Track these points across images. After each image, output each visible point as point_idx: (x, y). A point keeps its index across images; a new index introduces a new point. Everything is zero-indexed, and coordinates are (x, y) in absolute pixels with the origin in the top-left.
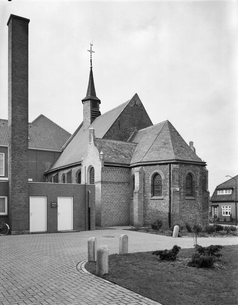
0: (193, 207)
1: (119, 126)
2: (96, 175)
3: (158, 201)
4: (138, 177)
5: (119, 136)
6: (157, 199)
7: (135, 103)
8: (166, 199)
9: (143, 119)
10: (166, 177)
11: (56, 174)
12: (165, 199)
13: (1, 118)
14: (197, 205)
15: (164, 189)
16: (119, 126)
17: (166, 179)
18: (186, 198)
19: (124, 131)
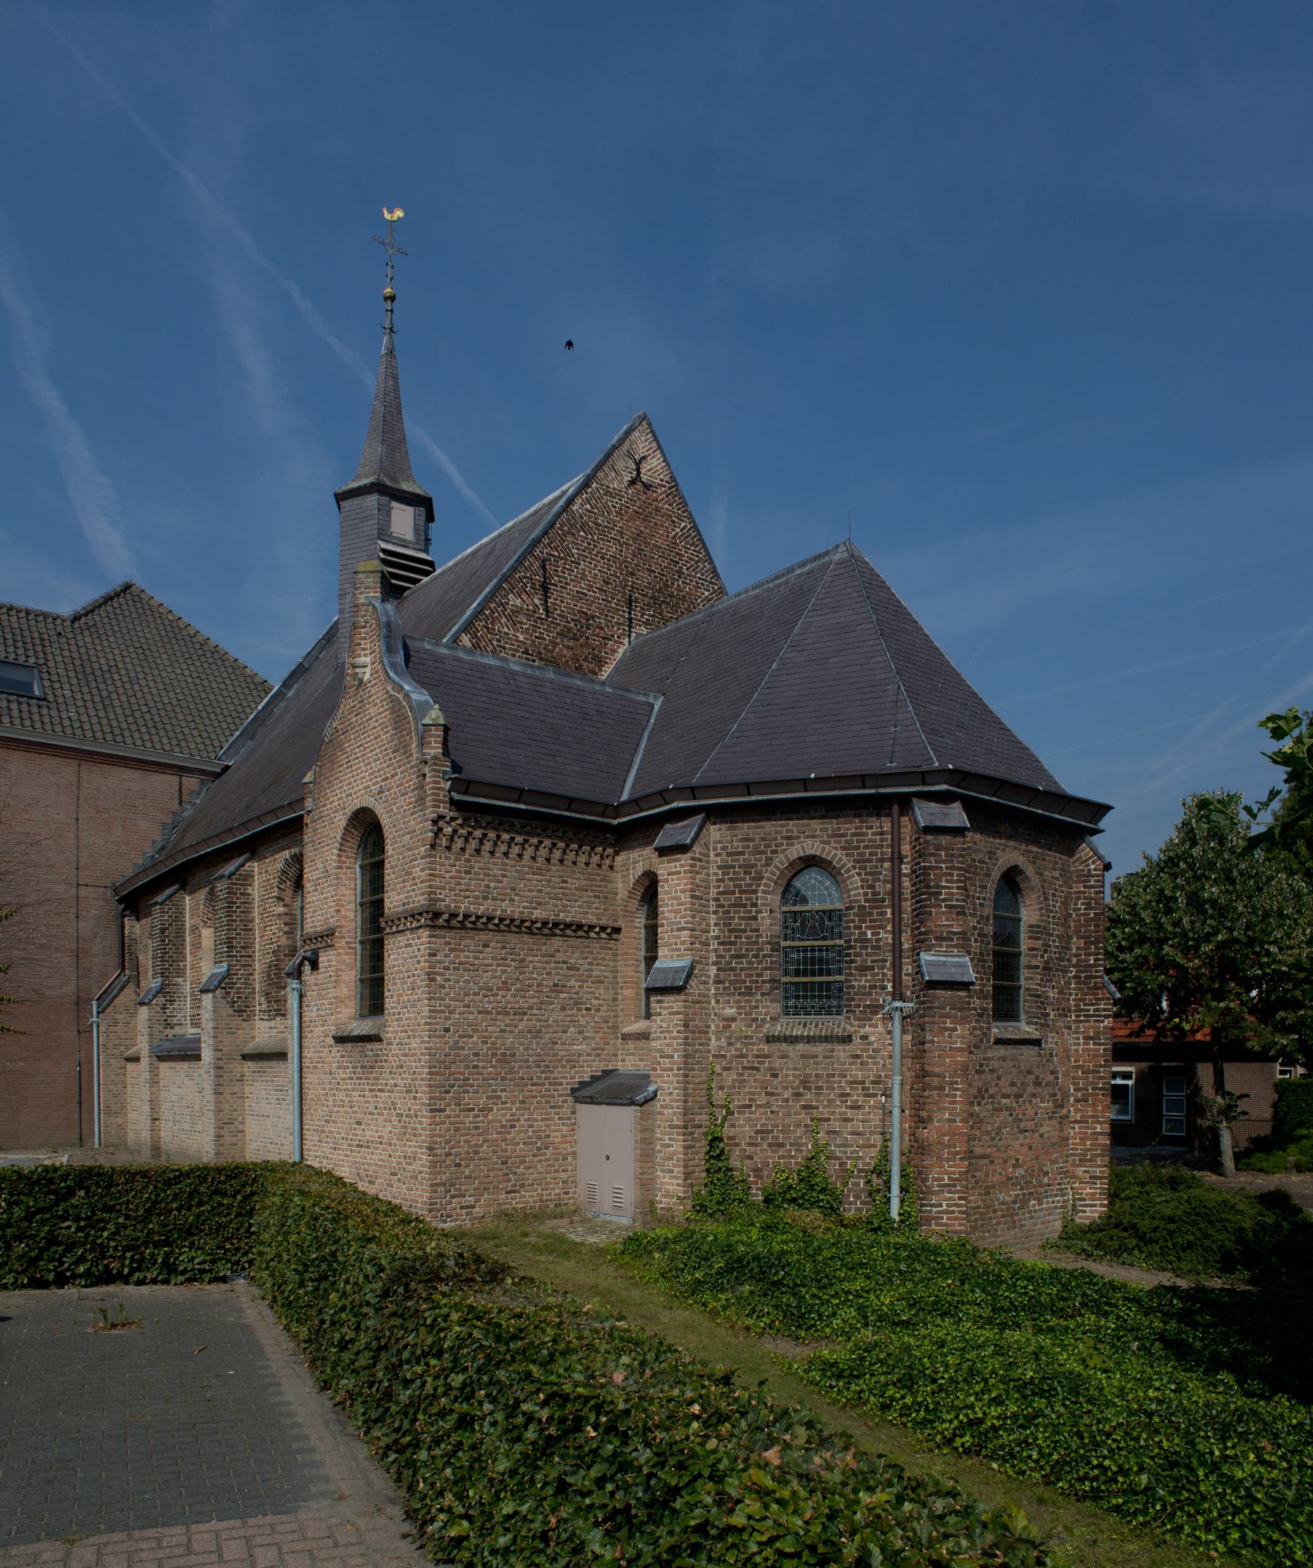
0: (1031, 1089)
1: (546, 598)
2: (1211, 1080)
3: (820, 1048)
4: (132, 1116)
5: (540, 653)
6: (809, 1040)
7: (638, 470)
8: (872, 1039)
9: (680, 572)
10: (872, 887)
11: (286, 854)
12: (864, 1038)
13: (8, 599)
14: (1051, 1078)
15: (864, 969)
16: (546, 598)
17: (876, 901)
18: (1115, 1069)
19: (569, 629)
